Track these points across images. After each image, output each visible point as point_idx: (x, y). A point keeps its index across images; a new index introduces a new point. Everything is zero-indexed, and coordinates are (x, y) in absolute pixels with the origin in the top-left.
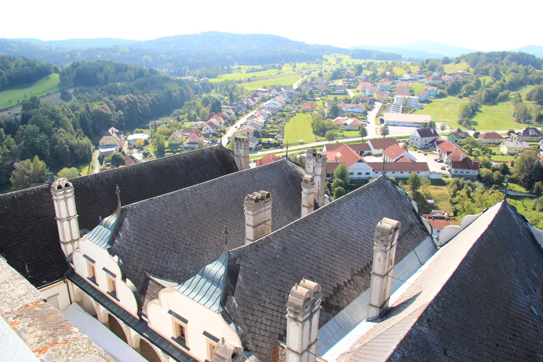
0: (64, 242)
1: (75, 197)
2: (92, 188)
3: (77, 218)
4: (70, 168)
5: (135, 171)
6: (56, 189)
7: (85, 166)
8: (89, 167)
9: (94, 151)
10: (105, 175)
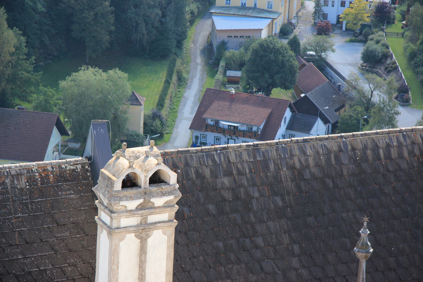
1: (178, 231)
2: (237, 198)
4: (105, 71)
5: (406, 155)
6: (118, 186)
9: (192, 22)
10: (292, 156)
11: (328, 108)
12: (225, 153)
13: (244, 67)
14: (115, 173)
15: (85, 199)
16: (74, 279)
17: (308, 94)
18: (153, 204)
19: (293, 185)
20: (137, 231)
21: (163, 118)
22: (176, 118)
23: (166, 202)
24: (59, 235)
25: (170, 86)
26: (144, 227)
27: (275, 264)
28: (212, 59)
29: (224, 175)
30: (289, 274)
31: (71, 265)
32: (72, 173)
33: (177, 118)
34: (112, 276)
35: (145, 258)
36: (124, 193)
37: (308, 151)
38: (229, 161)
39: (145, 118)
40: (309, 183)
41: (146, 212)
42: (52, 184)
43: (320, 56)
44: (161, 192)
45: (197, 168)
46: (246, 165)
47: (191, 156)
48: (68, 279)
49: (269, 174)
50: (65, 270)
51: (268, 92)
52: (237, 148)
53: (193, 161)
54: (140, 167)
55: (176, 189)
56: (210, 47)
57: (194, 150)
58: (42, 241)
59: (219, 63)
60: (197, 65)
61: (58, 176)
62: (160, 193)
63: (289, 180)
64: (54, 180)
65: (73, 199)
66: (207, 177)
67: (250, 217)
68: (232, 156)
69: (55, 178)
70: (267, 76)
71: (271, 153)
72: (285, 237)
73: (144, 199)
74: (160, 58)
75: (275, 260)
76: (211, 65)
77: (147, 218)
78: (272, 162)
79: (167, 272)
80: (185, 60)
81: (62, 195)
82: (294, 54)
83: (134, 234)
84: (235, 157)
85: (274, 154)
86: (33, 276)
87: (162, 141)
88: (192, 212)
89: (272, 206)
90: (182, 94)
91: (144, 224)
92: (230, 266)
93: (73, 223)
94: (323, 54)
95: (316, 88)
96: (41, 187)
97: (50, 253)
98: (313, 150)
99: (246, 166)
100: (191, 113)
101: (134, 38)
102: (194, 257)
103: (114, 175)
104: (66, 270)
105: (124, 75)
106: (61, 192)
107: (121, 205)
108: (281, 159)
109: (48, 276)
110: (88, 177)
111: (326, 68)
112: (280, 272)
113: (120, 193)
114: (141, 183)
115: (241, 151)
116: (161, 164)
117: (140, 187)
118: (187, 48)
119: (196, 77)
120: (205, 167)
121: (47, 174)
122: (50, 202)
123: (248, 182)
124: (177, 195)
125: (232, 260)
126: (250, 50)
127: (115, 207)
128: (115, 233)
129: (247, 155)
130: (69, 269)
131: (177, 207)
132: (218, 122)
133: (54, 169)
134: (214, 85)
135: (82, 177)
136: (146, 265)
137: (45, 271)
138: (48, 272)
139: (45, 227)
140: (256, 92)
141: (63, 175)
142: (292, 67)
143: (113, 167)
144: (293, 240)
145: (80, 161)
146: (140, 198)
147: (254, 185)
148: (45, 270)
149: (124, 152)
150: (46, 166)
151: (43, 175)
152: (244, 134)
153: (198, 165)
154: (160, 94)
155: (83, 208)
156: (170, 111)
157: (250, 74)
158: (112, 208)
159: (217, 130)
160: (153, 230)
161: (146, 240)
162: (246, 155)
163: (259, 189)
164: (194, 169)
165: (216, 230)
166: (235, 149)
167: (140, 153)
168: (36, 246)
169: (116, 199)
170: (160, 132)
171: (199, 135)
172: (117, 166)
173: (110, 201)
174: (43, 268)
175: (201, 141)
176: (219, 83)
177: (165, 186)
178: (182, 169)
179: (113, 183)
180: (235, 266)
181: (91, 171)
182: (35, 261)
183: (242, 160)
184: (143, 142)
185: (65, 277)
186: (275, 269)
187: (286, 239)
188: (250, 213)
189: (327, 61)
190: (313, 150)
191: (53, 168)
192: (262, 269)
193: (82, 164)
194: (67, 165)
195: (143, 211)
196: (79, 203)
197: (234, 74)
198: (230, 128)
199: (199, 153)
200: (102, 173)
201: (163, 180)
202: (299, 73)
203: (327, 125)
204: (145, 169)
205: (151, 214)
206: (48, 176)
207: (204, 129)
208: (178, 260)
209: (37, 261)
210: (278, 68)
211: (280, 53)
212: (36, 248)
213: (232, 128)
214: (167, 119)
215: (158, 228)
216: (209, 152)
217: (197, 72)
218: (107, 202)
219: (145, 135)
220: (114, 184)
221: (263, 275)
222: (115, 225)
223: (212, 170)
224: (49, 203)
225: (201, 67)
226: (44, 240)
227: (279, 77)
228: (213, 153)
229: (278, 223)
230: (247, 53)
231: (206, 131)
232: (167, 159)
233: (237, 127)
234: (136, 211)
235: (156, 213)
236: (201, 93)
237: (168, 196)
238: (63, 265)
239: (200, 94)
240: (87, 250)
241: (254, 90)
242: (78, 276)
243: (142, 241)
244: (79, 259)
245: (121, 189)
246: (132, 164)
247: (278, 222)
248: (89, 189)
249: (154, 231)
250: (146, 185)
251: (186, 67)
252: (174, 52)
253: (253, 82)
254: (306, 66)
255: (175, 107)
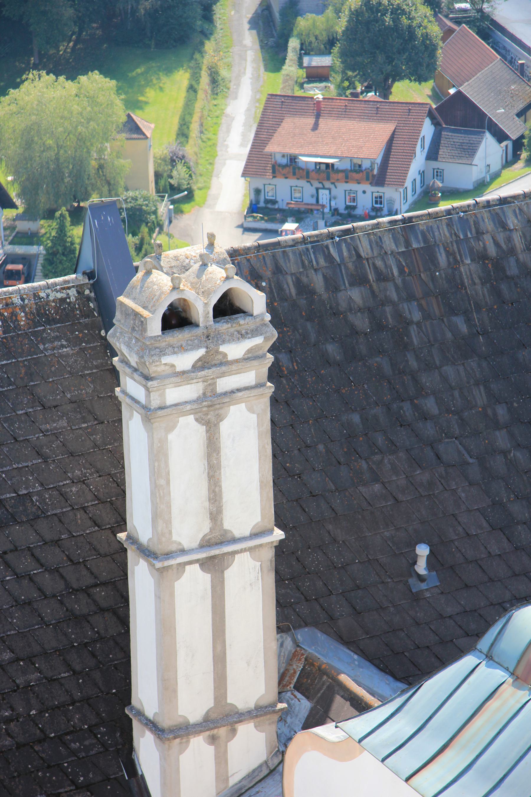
0: (165, 723)
1: (274, 401)
3: (269, 554)
4: (72, 77)
7: (169, 71)
8: (196, 76)
10: (479, 233)
11: (503, 110)
12: (349, 240)
13: (335, 46)
14: (146, 303)
15: (90, 355)
16: (85, 507)
17: (462, 87)
18: (225, 355)
19: (485, 290)
20: (198, 410)
21: (190, 161)
22: (215, 157)
23: (248, 350)
24: (48, 426)
25: (198, 96)
26: (211, 401)
27: (464, 447)
28: (273, 36)
29: (352, 284)
30: (492, 463)
31: (75, 481)
32: (60, 306)
33: (217, 158)
34: (158, 499)
35: (218, 459)
36: (167, 340)
37: (510, 220)
38: (359, 256)
39: (157, 162)
40: (516, 284)
41: (213, 372)
42: (24, 330)
43: (481, 11)
44: (238, 332)
45: (298, 275)
46: (392, 260)
47: (284, 252)
48: (73, 509)
49: (437, 274)
50: (65, 493)
51: (385, 92)
52: (372, 229)
53: (289, 261)
54: (194, 286)
55: (266, 323)
56: (266, 12)
57: (289, 240)
58: (16, 440)
59: (287, 42)
60: (246, 51)
61: (34, 314)
62: (236, 333)
63: (477, 281)
64: (28, 322)
65: (67, 356)
66: (318, 291)
67: (407, 361)
68: (364, 245)
69: (29, 319)
70: (381, 58)
71: (438, 233)
72: (478, 392)
73: (207, 348)
74: (174, 44)
75: (461, 438)
76: (272, 47)
77: (215, 383)
78: (442, 250)
79: (261, 482)
80: (221, 44)
81: (46, 349)
82: (431, 11)
83: (192, 417)
84: (369, 247)
85: (444, 234)
86: (8, 507)
87: (192, 203)
88: (296, 361)
89: (449, 335)
90: (222, 110)
91: (210, 396)
92: (378, 457)
93: (72, 402)
94: (485, 5)
95: (477, 74)
96: (5, 338)
97: (34, 462)
98: (519, 217)
99: (392, 262)
100: (242, 145)
101: (121, 8)
102: (307, 446)
103: (144, 308)
104: (68, 492)
105: (108, 84)
106: (44, 345)
107: (164, 364)
108: (458, 242)
109: (35, 505)
110: (92, 311)
111: (495, 33)
112: (474, 461)
113: (159, 341)
114: (199, 318)
115: (379, 234)
116: (233, 278)
117: (197, 326)
118: (224, 20)
119: (244, 73)
120: (313, 272)
121: (13, 311)
122: (25, 366)
123: (398, 294)
124: (268, 334)
125: (381, 445)
126: (344, 11)
127: (153, 368)
128: (158, 417)
129: (392, 241)
130: (74, 489)
131: (270, 357)
132: (295, 159)
133: (26, 301)
134: (281, 86)
135: (81, 311)
136: (220, 473)
137: (28, 497)
138: (35, 497)
139: (21, 414)
140: (362, 93)
141: (43, 312)
142: (426, 36)
143: (140, 292)
144: (495, 397)
145: (73, 281)
146: (199, 347)
147: (411, 297)
148: (29, 495)
149: (159, 259)
150: (10, 298)
151: (6, 314)
152: (347, 177)
153: (299, 269)
154: (179, 113)
155: (88, 372)
156: (202, 145)
157: (349, 59)
158: (147, 370)
159: (294, 174)
160: (229, 406)
161: (217, 425)
162: (390, 241)
163: (421, 305)
164: (292, 278)
165: (344, 391)
166: (368, 233)
167: (189, 258)
168: (7, 451)
169: (152, 353)
170: (188, 188)
171: (261, 187)
172: (148, 288)
173: (142, 357)
174: (25, 492)
175: (267, 198)
176: (289, 82)
177: (245, 319)
178: (270, 281)
179: (144, 322)
180: (387, 456)
181: (97, 299)
182: (7, 478)
183: (384, 251)
184: (157, 209)
185: (67, 504)
186: (464, 455)
187: (481, 395)
188: (407, 353)
189: (495, 19)
190: (519, 217)
191: (23, 299)
192: (439, 458)
193: (77, 286)
194: (49, 291)
195: (206, 371)
196: (80, 363)
197: (317, 62)
198: (320, 167)
199: (299, 244)
200: (122, 303)
201: (239, 307)
202: (442, 48)
203: (504, 144)
204: (203, 290)
205: (223, 375)
206: (16, 316)
207: (269, 174)
208: (276, 455)
209: (11, 480)
210: (402, 41)
211: (404, 12)
212: (7, 456)
213: (323, 167)
214: (197, 160)
215: (238, 402)
216: (318, 241)
217: (246, 63)
218: (136, 360)
219: (159, 196)
220: (146, 324)
221: (442, 470)
222: (155, 403)
223: (328, 276)
224: (22, 367)
225: (253, 53)
226: (21, 439)
227: (405, 59)
228: (325, 243)
229: (463, 367)
230: (340, 17)
231: (274, 177)
232: (238, 263)
233: (333, 165)
234: (193, 372)
235: (230, 373)
236: (257, 105)
237: (252, 339)
238: (62, 482)
239: (256, 107)
240: (104, 451)
241: (359, 90)
242: (91, 501)
243: (210, 428)
244: (89, 469)
245: (160, 333)
246: (177, 282)
247: (463, 364)
248: (96, 334)
249: (231, 407)
250: (208, 321)
251: (225, 57)
252: (199, 30)
253: (355, 73)
254: (454, 32)
255: (210, 136)
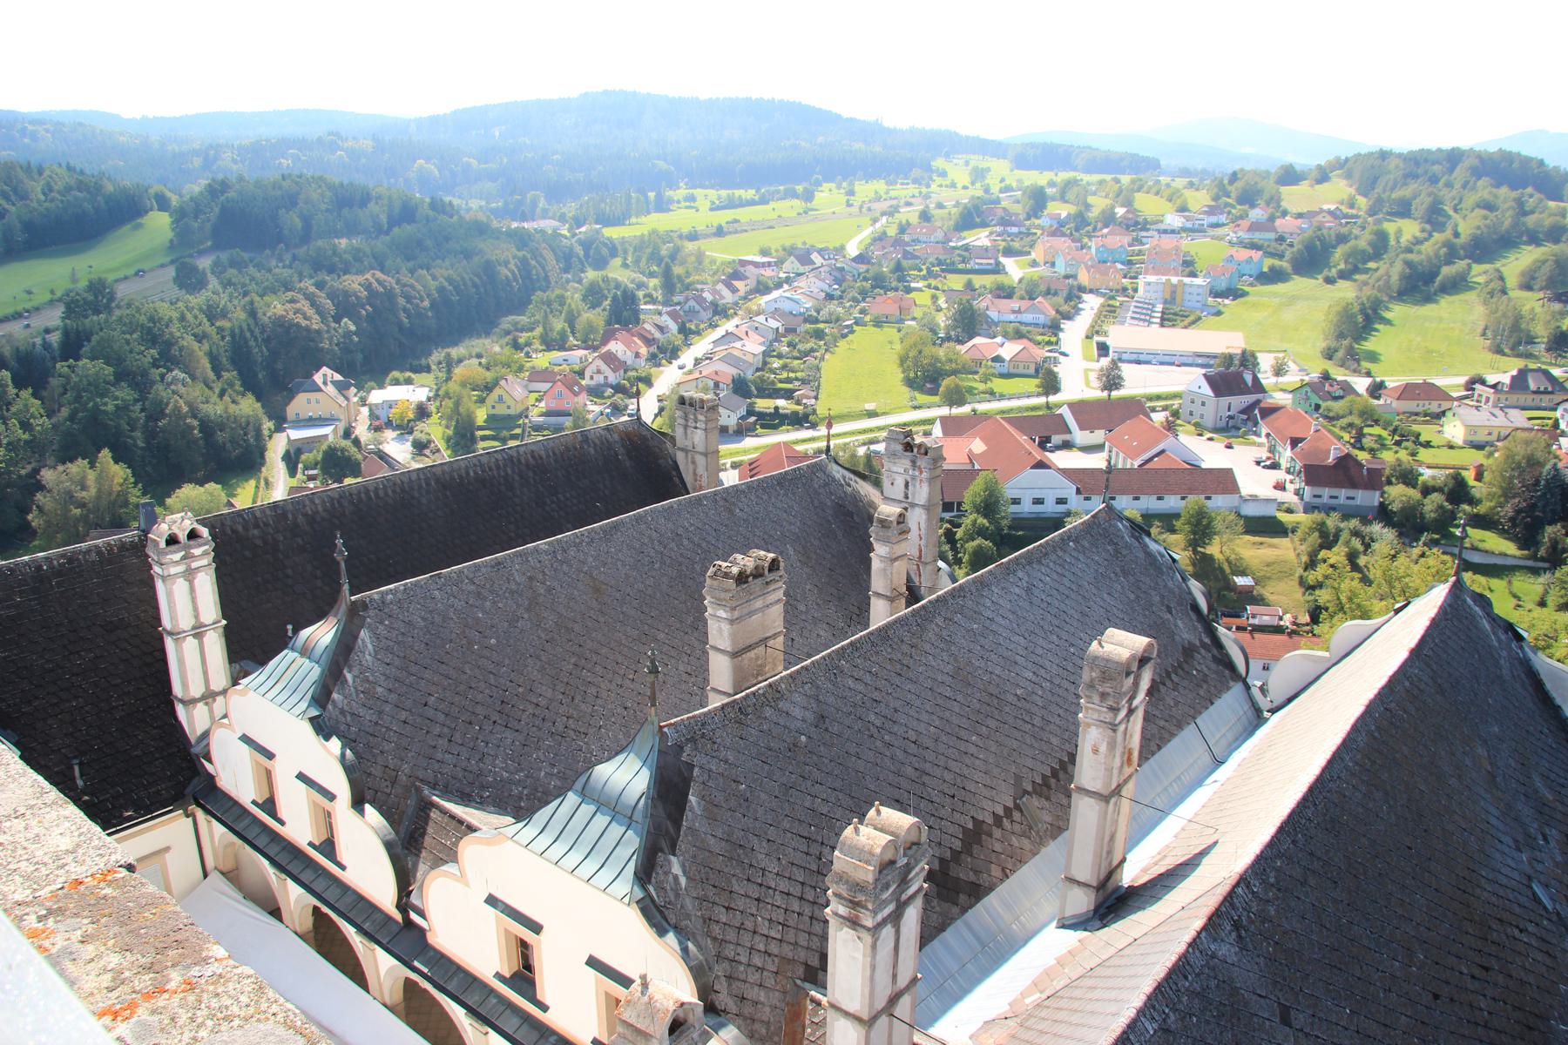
0: (186, 699)
1: (216, 569)
2: (266, 543)
3: (221, 630)
4: (202, 485)
5: (390, 492)
6: (163, 544)
7: (247, 480)
8: (258, 482)
9: (270, 437)
10: (304, 506)
